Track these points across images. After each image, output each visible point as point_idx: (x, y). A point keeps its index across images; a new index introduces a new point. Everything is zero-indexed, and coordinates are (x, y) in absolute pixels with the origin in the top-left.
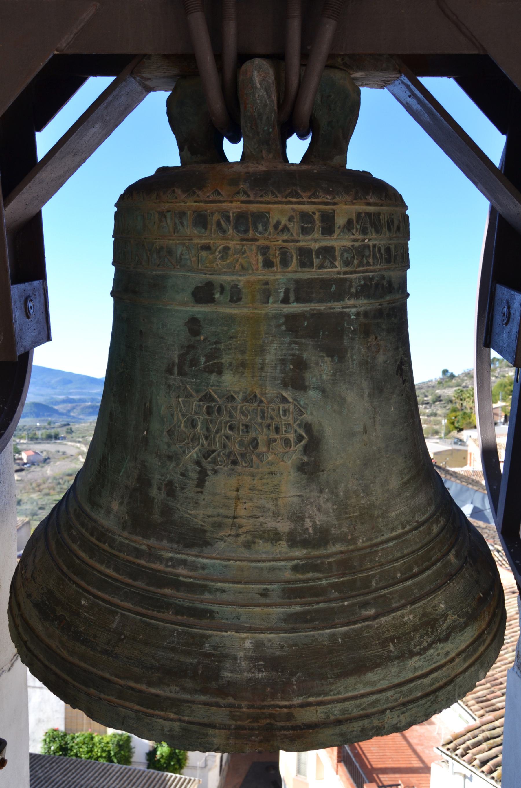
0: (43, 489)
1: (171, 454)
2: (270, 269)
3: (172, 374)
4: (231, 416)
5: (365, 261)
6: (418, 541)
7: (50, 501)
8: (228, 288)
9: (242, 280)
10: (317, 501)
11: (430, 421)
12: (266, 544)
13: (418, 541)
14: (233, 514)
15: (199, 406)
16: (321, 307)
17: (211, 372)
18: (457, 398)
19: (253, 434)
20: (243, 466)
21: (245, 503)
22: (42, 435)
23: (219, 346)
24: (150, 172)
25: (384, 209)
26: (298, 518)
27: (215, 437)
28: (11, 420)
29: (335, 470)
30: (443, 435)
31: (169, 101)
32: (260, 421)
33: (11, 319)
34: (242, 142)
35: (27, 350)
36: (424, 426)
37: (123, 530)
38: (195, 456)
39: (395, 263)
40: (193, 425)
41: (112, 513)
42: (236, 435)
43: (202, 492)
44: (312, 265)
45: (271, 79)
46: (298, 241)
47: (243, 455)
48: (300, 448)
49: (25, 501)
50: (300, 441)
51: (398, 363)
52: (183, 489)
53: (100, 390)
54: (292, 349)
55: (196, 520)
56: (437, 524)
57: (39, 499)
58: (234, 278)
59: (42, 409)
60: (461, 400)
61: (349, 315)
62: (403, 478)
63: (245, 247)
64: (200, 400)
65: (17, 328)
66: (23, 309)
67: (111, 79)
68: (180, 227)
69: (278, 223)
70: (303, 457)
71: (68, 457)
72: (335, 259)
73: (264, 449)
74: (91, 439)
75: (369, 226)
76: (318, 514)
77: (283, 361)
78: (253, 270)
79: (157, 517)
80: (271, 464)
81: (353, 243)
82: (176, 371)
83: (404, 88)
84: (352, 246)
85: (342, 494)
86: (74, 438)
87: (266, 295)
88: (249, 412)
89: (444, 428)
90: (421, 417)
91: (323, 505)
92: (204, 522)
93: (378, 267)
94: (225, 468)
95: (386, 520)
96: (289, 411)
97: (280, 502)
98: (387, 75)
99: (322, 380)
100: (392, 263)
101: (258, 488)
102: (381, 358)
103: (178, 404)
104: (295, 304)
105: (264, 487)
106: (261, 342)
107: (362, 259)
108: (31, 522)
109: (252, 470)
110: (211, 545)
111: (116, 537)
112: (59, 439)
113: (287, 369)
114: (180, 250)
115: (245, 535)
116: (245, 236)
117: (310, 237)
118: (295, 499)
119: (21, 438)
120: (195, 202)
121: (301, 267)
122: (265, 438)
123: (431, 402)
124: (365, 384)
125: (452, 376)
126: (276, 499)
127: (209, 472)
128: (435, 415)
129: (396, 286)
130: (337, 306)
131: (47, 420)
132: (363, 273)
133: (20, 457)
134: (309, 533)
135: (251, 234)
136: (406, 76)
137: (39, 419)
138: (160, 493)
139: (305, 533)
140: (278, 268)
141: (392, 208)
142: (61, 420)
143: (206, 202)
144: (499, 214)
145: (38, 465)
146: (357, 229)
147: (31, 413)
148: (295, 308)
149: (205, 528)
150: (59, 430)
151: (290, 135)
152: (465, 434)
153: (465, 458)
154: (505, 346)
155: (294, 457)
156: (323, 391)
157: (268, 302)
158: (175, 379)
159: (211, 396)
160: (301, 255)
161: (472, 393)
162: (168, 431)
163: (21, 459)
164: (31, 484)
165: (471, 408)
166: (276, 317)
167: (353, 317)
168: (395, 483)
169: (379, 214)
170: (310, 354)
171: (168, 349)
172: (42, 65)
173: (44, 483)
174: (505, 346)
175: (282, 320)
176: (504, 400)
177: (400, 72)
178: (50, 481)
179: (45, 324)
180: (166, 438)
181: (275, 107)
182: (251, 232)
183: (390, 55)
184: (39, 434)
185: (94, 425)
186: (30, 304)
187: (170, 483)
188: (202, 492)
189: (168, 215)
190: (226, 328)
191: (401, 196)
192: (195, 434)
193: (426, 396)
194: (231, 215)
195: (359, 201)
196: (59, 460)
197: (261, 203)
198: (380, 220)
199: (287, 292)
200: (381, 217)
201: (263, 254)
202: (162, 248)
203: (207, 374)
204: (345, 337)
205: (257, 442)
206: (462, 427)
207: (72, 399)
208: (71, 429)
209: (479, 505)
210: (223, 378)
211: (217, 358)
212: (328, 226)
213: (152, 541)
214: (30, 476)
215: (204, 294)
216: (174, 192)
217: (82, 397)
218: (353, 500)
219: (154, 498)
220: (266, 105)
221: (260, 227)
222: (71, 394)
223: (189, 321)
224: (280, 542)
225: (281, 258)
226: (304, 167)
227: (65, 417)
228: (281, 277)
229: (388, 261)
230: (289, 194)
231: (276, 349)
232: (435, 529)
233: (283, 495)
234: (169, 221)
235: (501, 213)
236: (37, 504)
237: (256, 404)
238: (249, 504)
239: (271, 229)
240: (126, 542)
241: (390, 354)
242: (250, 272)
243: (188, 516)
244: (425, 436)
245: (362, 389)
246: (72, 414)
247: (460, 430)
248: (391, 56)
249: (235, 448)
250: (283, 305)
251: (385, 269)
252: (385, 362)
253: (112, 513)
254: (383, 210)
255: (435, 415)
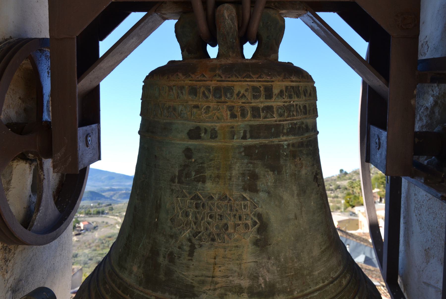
0: (92, 246)
1: (172, 234)
2: (235, 119)
3: (174, 182)
4: (211, 209)
5: (292, 114)
6: (333, 291)
7: (96, 255)
8: (209, 130)
9: (217, 126)
10: (267, 265)
11: (334, 201)
12: (234, 296)
13: (333, 291)
14: (211, 275)
15: (191, 203)
16: (265, 141)
17: (198, 181)
18: (350, 187)
19: (225, 221)
20: (218, 242)
21: (220, 267)
22: (94, 211)
23: (203, 165)
24: (163, 63)
25: (302, 84)
26: (254, 277)
27: (200, 223)
28: (72, 209)
29: (277, 244)
30: (343, 210)
31: (176, 25)
32: (229, 212)
33: (77, 148)
34: (217, 46)
35: (85, 166)
36: (331, 204)
37: (140, 286)
38: (188, 235)
39: (309, 114)
40: (187, 215)
41: (132, 275)
42: (214, 222)
43: (191, 260)
44: (260, 117)
45: (234, 14)
46: (251, 103)
47: (218, 235)
48: (255, 230)
49: (81, 254)
50: (255, 225)
51: (314, 174)
52: (180, 257)
53: (131, 183)
54: (249, 167)
55: (187, 279)
56: (345, 278)
57: (89, 253)
58: (213, 124)
59: (95, 195)
60: (352, 188)
61: (283, 146)
62: (321, 248)
63: (220, 106)
64: (192, 199)
65: (80, 153)
66: (85, 142)
67: (144, 14)
68: (181, 95)
69: (239, 92)
70: (257, 236)
71: (109, 226)
72: (273, 112)
73: (232, 231)
74: (125, 214)
75: (293, 93)
76: (268, 274)
77: (243, 175)
78: (224, 120)
79: (162, 277)
80: (237, 240)
81: (284, 104)
82: (177, 180)
83: (309, 18)
84: (283, 105)
85: (282, 260)
86: (114, 214)
87: (233, 134)
88: (222, 207)
89: (343, 205)
90: (329, 199)
91: (271, 268)
92: (193, 280)
93: (299, 117)
94: (207, 244)
95: (312, 277)
96: (247, 206)
97: (243, 266)
98: (299, 12)
99: (267, 186)
100: (308, 114)
101: (228, 257)
102: (303, 172)
103: (178, 201)
104: (250, 140)
105: (232, 256)
106: (230, 163)
107: (290, 112)
108: (83, 269)
109: (224, 244)
110: (198, 296)
111: (135, 290)
112: (104, 214)
113: (246, 179)
114: (180, 108)
115: (220, 289)
116: (219, 100)
117: (258, 100)
118: (252, 264)
119: (81, 213)
120: (190, 81)
121: (253, 118)
122: (233, 223)
123: (334, 189)
124: (294, 188)
125: (346, 173)
126: (240, 264)
127: (196, 246)
128: (337, 197)
129: (310, 127)
130: (276, 141)
131: (97, 202)
132: (291, 120)
133: (79, 225)
134: (262, 287)
135: (223, 99)
136: (310, 12)
137: (93, 201)
138: (165, 260)
139: (259, 287)
140: (239, 118)
141: (306, 83)
142: (106, 202)
143: (196, 81)
144: (369, 86)
145: (90, 231)
146: (286, 96)
147: (88, 198)
148: (250, 142)
149: (193, 284)
150: (105, 208)
151: (245, 43)
152: (357, 209)
153: (357, 225)
154: (379, 162)
155: (251, 236)
156: (269, 193)
157: (234, 139)
158: (176, 186)
159: (198, 196)
160: (253, 111)
161: (358, 183)
162: (171, 219)
163: (80, 227)
164: (85, 243)
165: (359, 193)
166: (239, 147)
167: (285, 147)
168: (316, 252)
169: (299, 87)
170: (260, 170)
171: (172, 167)
172: (105, 7)
173: (93, 242)
174: (379, 162)
175: (242, 149)
176: (378, 187)
177: (307, 10)
178: (97, 241)
179: (98, 150)
180: (169, 224)
181: (237, 29)
182: (223, 97)
183: (300, 2)
184: (92, 211)
185: (127, 205)
186: (89, 138)
187: (171, 254)
188: (191, 260)
189: (174, 88)
190: (208, 154)
191: (311, 76)
192: (188, 221)
193: (331, 186)
194: (211, 88)
195: (287, 79)
196: (103, 227)
197: (229, 81)
198: (299, 90)
199: (245, 132)
200: (300, 88)
201: (230, 110)
202: (170, 107)
203: (196, 183)
204: (281, 159)
205: (228, 226)
206: (354, 205)
207: (114, 189)
208: (112, 208)
209: (369, 255)
210: (206, 185)
211: (202, 172)
212: (269, 94)
213: (158, 293)
214: (84, 238)
215: (195, 134)
216: (178, 75)
217: (120, 187)
218: (290, 264)
219: (160, 264)
220: (231, 28)
221: (229, 95)
222: (113, 185)
223: (185, 150)
224: (243, 294)
225: (241, 113)
226: (254, 61)
227: (109, 200)
228: (241, 124)
229: (305, 113)
230: (245, 76)
231: (239, 167)
232: (344, 282)
233: (244, 261)
234: (174, 91)
235: (370, 85)
236: (88, 257)
237: (226, 202)
238: (223, 268)
239: (235, 96)
240: (142, 294)
241: (309, 169)
242: (223, 121)
243: (183, 276)
244: (331, 210)
245: (293, 191)
246: (113, 198)
247: (353, 207)
248: (301, 2)
249: (214, 230)
250: (243, 140)
251: (304, 118)
252: (306, 174)
253: (132, 275)
254: (301, 85)
255: (337, 197)
